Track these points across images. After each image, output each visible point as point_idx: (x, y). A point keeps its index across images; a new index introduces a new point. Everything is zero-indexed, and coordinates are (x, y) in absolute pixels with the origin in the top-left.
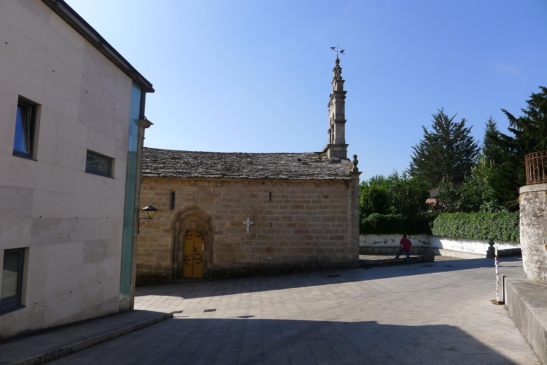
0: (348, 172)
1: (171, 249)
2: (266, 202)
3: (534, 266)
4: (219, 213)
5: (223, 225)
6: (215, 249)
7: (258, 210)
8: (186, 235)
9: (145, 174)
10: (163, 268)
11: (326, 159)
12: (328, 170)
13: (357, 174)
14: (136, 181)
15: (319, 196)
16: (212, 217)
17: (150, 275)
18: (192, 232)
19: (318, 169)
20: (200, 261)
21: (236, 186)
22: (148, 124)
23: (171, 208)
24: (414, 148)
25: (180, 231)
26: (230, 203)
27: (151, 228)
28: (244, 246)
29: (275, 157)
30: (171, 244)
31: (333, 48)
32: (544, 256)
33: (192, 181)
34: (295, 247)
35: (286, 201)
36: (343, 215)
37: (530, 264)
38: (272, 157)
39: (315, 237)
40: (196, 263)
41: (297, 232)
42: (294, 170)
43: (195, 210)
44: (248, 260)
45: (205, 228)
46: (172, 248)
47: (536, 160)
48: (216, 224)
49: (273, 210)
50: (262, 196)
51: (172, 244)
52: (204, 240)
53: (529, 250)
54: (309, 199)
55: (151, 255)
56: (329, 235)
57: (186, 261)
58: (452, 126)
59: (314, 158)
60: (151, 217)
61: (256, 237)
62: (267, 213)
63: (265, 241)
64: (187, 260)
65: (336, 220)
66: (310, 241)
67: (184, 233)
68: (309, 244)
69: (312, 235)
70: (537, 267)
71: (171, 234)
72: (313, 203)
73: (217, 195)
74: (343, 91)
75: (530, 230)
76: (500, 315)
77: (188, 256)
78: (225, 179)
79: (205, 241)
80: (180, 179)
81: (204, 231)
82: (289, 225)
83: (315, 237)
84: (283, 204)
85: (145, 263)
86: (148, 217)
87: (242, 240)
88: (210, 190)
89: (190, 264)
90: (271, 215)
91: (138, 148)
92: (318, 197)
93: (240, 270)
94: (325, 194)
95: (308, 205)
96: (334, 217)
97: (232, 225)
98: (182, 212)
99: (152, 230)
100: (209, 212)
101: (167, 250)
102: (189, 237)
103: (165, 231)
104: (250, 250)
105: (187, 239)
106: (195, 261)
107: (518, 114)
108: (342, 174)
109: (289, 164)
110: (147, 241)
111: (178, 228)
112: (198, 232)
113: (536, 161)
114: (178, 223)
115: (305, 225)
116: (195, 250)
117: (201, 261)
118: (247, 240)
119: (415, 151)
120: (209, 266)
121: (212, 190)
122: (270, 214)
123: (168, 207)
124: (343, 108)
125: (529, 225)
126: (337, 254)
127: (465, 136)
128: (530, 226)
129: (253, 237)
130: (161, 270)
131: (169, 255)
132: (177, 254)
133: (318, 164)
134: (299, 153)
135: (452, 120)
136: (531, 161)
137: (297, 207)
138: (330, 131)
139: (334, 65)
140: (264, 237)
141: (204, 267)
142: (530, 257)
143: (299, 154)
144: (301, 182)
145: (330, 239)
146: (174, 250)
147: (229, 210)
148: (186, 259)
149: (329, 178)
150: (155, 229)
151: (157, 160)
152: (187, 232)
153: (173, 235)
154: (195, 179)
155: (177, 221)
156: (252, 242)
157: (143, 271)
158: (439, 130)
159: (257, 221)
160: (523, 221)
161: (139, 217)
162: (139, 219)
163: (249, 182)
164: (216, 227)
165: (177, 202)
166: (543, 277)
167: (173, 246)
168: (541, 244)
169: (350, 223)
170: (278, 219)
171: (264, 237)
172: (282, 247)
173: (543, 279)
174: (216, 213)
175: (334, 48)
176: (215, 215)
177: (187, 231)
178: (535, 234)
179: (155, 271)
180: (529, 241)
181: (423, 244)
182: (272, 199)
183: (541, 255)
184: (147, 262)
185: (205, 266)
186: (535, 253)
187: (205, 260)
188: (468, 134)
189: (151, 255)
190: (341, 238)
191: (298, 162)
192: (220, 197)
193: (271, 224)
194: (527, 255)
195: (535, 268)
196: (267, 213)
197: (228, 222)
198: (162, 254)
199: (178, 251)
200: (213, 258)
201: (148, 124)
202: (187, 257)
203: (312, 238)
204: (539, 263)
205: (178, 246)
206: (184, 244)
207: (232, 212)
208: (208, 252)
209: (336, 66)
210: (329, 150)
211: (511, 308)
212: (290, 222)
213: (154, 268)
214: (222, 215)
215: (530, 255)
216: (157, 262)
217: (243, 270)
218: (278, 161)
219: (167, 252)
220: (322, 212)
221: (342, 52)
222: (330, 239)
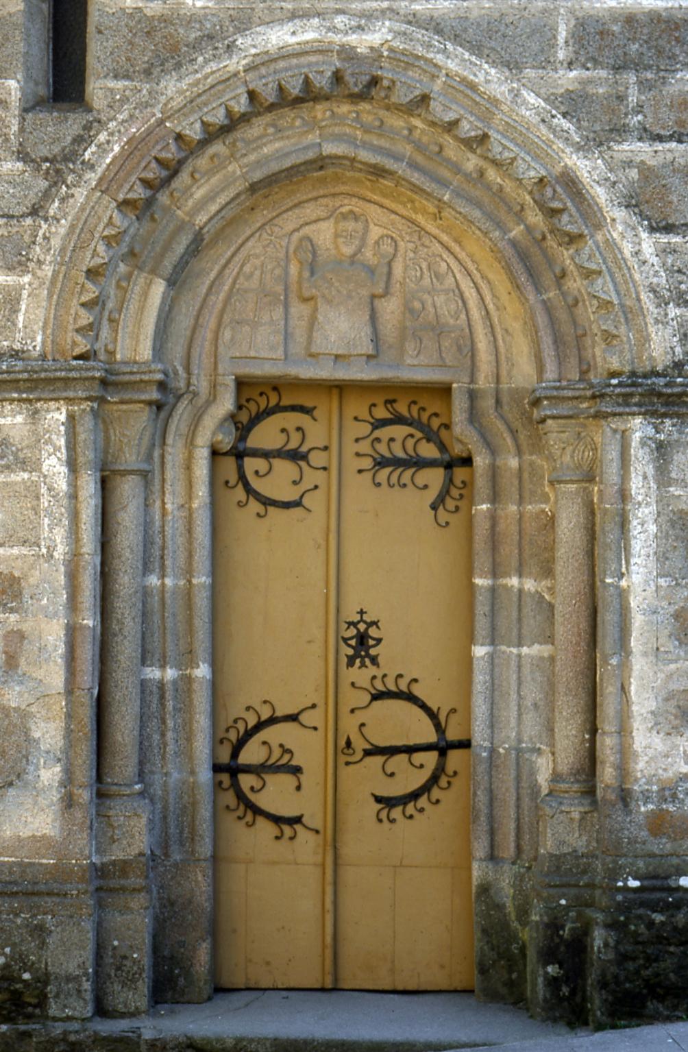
8: (239, 454)
23: (43, 91)
40: (378, 799)
45: (482, 344)
57: (246, 781)
64: (259, 770)
77: (273, 720)
89: (298, 820)
98: (194, 132)
105: (254, 506)
116: (362, 638)
117: (434, 779)
148: (252, 754)
202: (260, 726)
205: (146, 592)
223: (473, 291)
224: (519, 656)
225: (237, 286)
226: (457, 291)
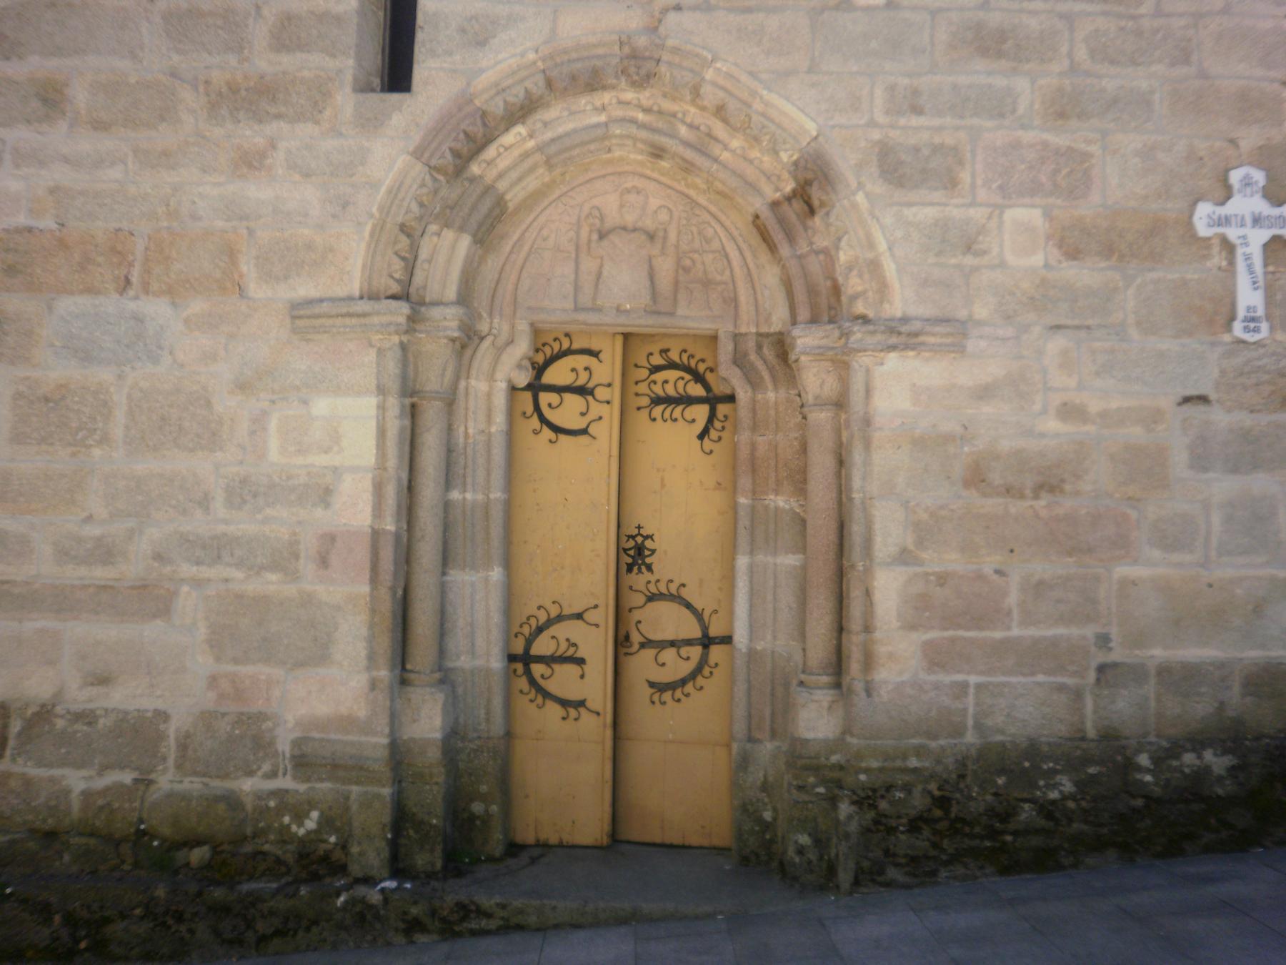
1: (376, 535)
4: (915, 121)
5: (968, 249)
10: (284, 745)
16: (845, 162)
18: (594, 354)
25: (468, 340)
26: (1034, 13)
27: (146, 288)
28: (1223, 486)
40: (652, 684)
43: (645, 97)
51: (381, 466)
57: (538, 669)
64: (549, 660)
71: (372, 355)
77: (560, 618)
81: (737, 338)
89: (581, 704)
93: (1189, 758)
97: (1073, 254)
99: (156, 309)
101: (330, 539)
102: (568, 411)
105: (547, 433)
110: (105, 440)
111: (451, 293)
112: (657, 360)
114: (449, 235)
116: (640, 549)
117: (698, 671)
118: (1246, 420)
130: (266, 767)
132: (443, 590)
147: (1022, 84)
150: (197, 306)
152: (540, 359)
157: (52, 780)
164: (890, 268)
167: (391, 492)
174: (881, 118)
176: (876, 135)
179: (192, 785)
184: (103, 680)
197: (1026, 215)
198: (271, 583)
199: (446, 559)
202: (550, 622)
205: (447, 505)
206: (510, 483)
213: (183, 747)
214: (949, 140)
216: (213, 680)
217: (1216, 762)
219: (323, 561)
223: (737, 253)
224: (775, 564)
225: (535, 246)
226: (722, 252)
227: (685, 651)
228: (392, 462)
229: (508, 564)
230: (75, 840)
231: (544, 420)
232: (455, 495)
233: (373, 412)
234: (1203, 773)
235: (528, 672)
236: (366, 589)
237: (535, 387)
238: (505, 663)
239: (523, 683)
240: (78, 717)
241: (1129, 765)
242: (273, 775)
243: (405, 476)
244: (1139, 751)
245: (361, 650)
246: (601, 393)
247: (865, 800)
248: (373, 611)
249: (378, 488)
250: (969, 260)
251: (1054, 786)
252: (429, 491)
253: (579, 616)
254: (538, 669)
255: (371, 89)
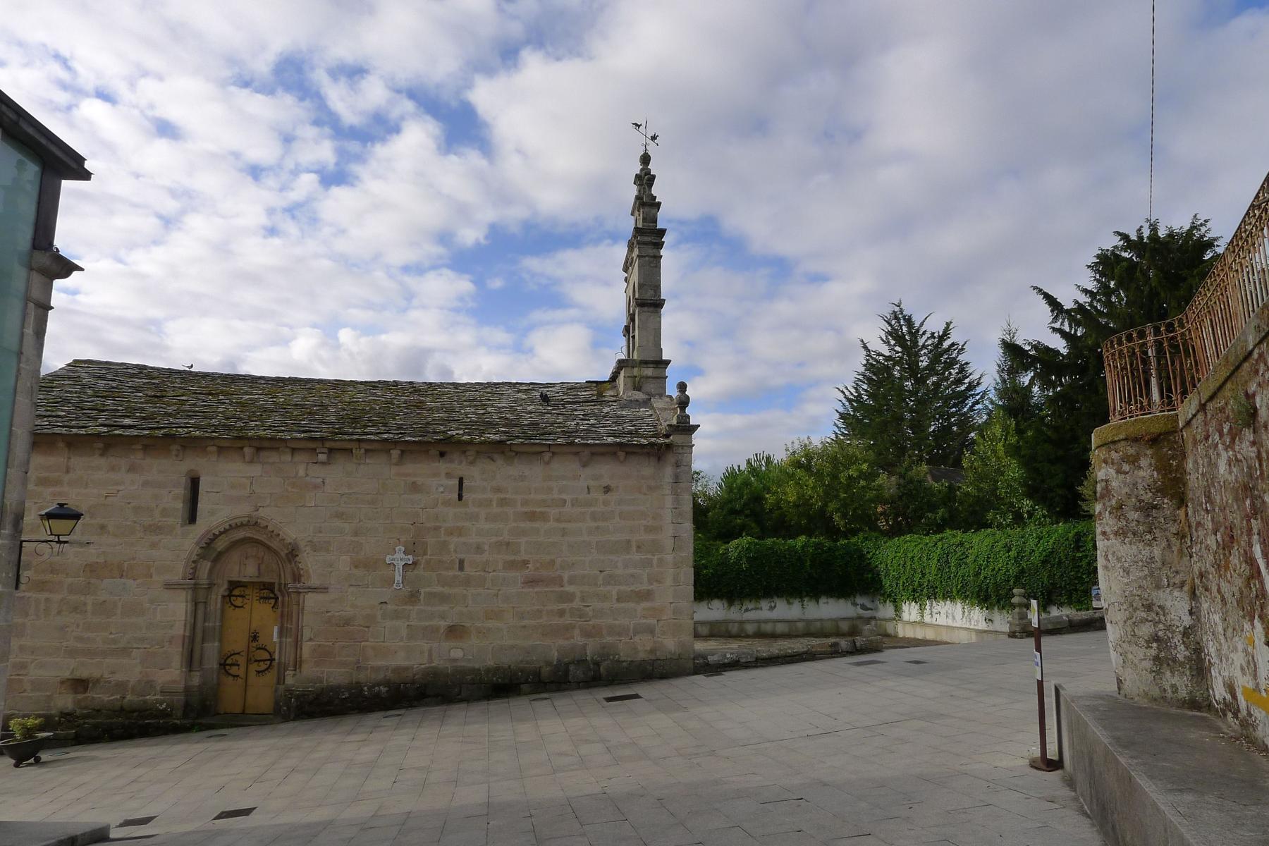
0: (663, 427)
1: (184, 636)
2: (447, 503)
3: (1141, 653)
6: (307, 634)
7: (428, 525)
8: (230, 596)
9: (115, 430)
10: (158, 688)
11: (613, 396)
12: (616, 422)
13: (689, 430)
14: (11, 431)
15: (588, 488)
16: (302, 544)
17: (122, 707)
19: (589, 420)
20: (266, 667)
21: (368, 461)
22: (66, 268)
24: (839, 390)
29: (485, 392)
30: (183, 622)
31: (636, 124)
32: (1169, 623)
33: (246, 450)
34: (526, 622)
35: (503, 502)
36: (651, 537)
37: (1130, 649)
38: (477, 391)
39: (578, 594)
40: (256, 671)
41: (532, 582)
42: (526, 422)
44: (400, 660)
46: (185, 631)
47: (1134, 349)
48: (311, 563)
49: (467, 524)
50: (437, 489)
52: (279, 610)
53: (1125, 607)
54: (564, 496)
55: (125, 651)
56: (614, 590)
57: (227, 667)
58: (925, 337)
59: (583, 393)
60: (62, 539)
61: (422, 597)
62: (450, 533)
63: (445, 608)
64: (231, 665)
65: (634, 549)
66: (564, 606)
67: (225, 590)
68: (561, 613)
69: (569, 588)
70: (1152, 658)
72: (573, 505)
73: (316, 487)
74: (658, 227)
75: (1127, 550)
76: (1056, 806)
78: (338, 443)
79: (282, 612)
80: (212, 443)
81: (280, 584)
82: (511, 565)
83: (578, 594)
84: (495, 509)
85: (106, 676)
86: (52, 538)
87: (384, 606)
88: (297, 474)
89: (238, 676)
90: (462, 539)
91: (22, 335)
92: (586, 490)
93: (377, 688)
94: (606, 481)
95: (560, 512)
96: (629, 541)
97: (356, 567)
98: (217, 533)
99: (130, 582)
100: (291, 533)
102: (239, 602)
103: (169, 586)
104: (404, 632)
105: (233, 607)
106: (254, 667)
107: (1069, 297)
108: (650, 431)
109: (518, 408)
111: (205, 578)
112: (262, 587)
113: (1134, 353)
115: (552, 562)
116: (255, 636)
117: (269, 666)
119: (841, 397)
120: (289, 680)
121: (302, 473)
122: (460, 535)
123: (176, 519)
124: (658, 269)
125: (1121, 533)
126: (637, 639)
127: (953, 362)
128: (1127, 539)
129: (413, 597)
130: (153, 693)
131: (176, 655)
132: (202, 649)
133: (593, 408)
134: (547, 384)
135: (922, 324)
136: (1119, 354)
137: (532, 516)
138: (627, 329)
139: (637, 168)
140: (444, 599)
141: (278, 683)
142: (1129, 629)
143: (547, 385)
144: (543, 452)
145: (618, 600)
146: (192, 639)
148: (229, 661)
149: (615, 440)
151: (163, 397)
153: (189, 597)
154: (256, 444)
155: (202, 557)
156: (410, 610)
157: (99, 698)
158: (895, 345)
159: (425, 553)
160: (1105, 524)
161: (23, 539)
162: (22, 542)
163: (403, 452)
165: (202, 505)
166: (1167, 687)
167: (188, 626)
168: (1158, 587)
169: (669, 557)
170: (479, 549)
171: (444, 599)
172: (490, 624)
173: (1169, 691)
174: (312, 535)
175: (639, 126)
177: (234, 585)
178: (1142, 561)
180: (1126, 581)
181: (861, 612)
182: (465, 495)
183: (1160, 622)
185: (280, 680)
186: (1144, 615)
187: (279, 663)
188: (960, 356)
189: (125, 651)
190: (647, 596)
191: (541, 405)
192: (323, 492)
193: (461, 562)
194: (1121, 624)
195: (1143, 660)
196: (450, 533)
199: (203, 640)
200: (301, 657)
201: (66, 268)
202: (231, 655)
203: (569, 597)
204: (1155, 645)
206: (222, 620)
207: (356, 534)
208: (289, 640)
209: (642, 170)
210: (622, 373)
211: (1080, 778)
212: (512, 558)
215: (1129, 622)
216: (141, 673)
217: (383, 689)
218: (490, 400)
219: (170, 642)
220: (598, 528)
221: (654, 138)
222: (618, 600)
227: (266, 663)
228: (189, 618)
229: (220, 641)
230: (105, 712)
231: (232, 604)
232: (207, 624)
233: (184, 607)
234: (380, 691)
235: (225, 668)
236: (181, 649)
237: (230, 596)
238: (218, 666)
239: (223, 671)
240: (106, 682)
241: (362, 690)
242: (155, 695)
243: (193, 621)
244: (365, 686)
245: (179, 664)
246: (247, 597)
247: (298, 697)
248: (182, 655)
249: (185, 625)
250: (331, 569)
251: (344, 695)
252: (199, 624)
253: (238, 654)
254: (227, 667)
255: (186, 524)
